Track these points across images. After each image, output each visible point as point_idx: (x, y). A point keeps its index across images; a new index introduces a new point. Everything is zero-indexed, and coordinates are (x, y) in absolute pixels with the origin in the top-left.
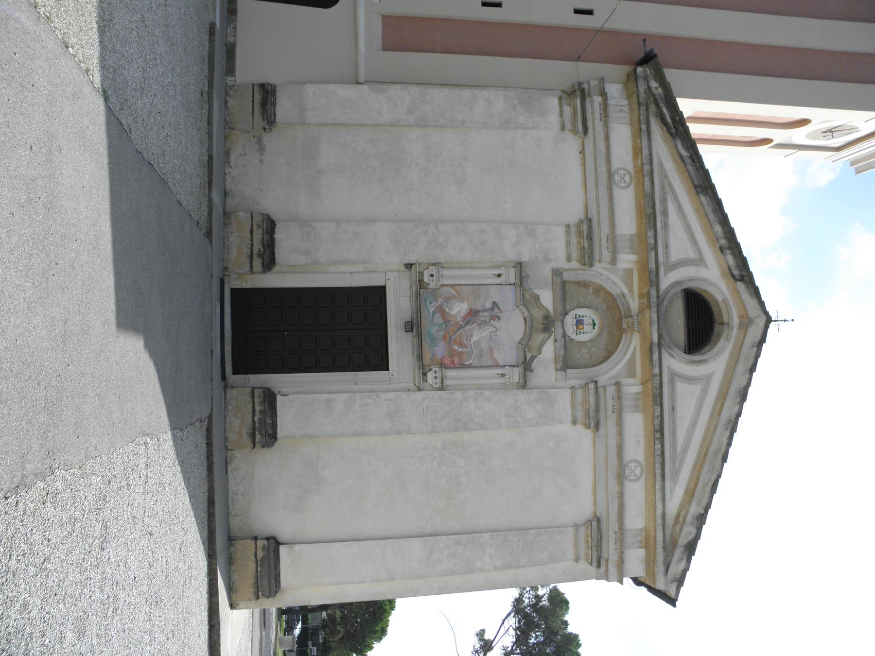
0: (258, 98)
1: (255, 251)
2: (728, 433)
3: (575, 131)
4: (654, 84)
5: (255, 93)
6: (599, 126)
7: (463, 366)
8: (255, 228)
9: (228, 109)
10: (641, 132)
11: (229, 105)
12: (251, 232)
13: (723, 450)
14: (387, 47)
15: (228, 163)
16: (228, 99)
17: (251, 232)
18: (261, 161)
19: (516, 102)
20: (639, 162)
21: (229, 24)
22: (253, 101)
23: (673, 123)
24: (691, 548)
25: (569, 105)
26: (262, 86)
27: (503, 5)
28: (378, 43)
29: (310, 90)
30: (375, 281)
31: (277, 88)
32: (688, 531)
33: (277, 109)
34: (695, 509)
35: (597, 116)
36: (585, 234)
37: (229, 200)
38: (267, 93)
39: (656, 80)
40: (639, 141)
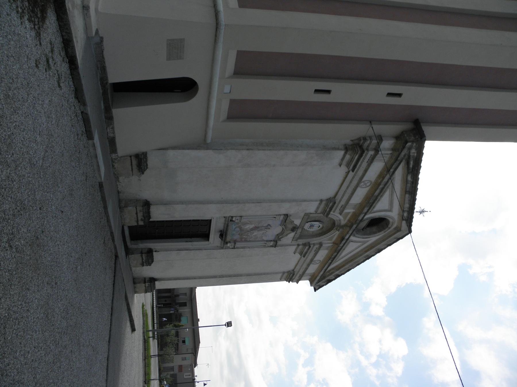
0: (134, 162)
1: (139, 218)
2: (365, 259)
3: (348, 165)
4: (413, 151)
6: (365, 164)
7: (246, 241)
8: (138, 212)
10: (389, 170)
12: (137, 214)
13: (360, 262)
15: (119, 181)
17: (137, 214)
18: (140, 180)
20: (380, 181)
23: (413, 168)
24: (330, 281)
25: (350, 155)
26: (137, 156)
29: (171, 153)
30: (207, 217)
32: (331, 277)
34: (337, 272)
35: (366, 160)
36: (330, 206)
37: (120, 195)
39: (416, 149)
40: (385, 173)
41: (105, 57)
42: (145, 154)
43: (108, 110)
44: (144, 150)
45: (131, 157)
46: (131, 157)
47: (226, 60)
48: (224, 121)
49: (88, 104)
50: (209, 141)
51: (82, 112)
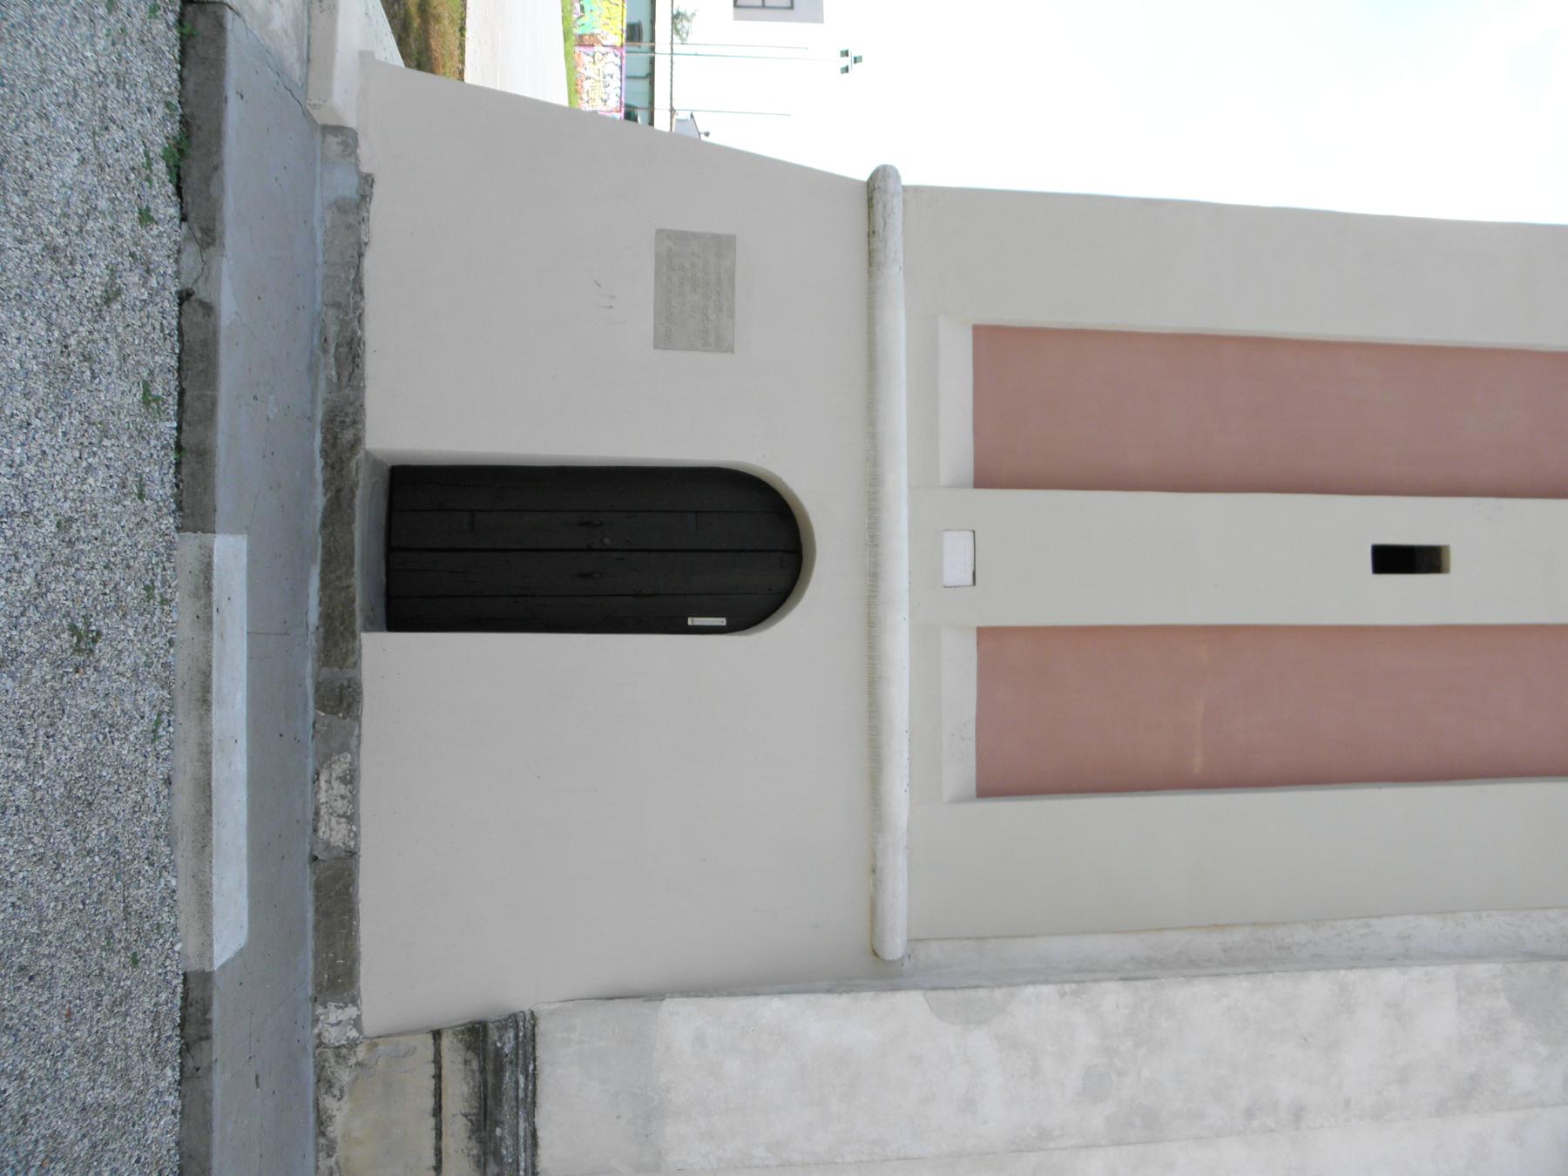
5: (449, 1144)
9: (330, 1150)
11: (335, 1130)
14: (996, 783)
16: (329, 1102)
19: (1502, 1002)
21: (325, 759)
22: (437, 1111)
26: (476, 1034)
27: (1455, 559)
28: (961, 770)
29: (682, 1021)
31: (542, 1027)
33: (541, 1119)
38: (499, 1071)
41: (369, 284)
42: (524, 1029)
43: (336, 639)
44: (519, 999)
45: (437, 1034)
46: (437, 1034)
47: (930, 409)
48: (960, 799)
49: (229, 240)
50: (895, 947)
51: (184, 297)
